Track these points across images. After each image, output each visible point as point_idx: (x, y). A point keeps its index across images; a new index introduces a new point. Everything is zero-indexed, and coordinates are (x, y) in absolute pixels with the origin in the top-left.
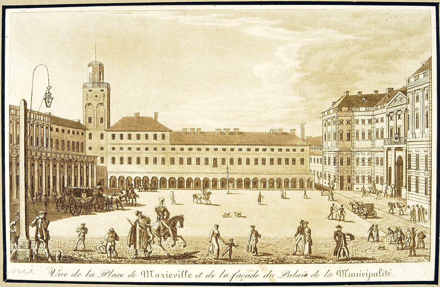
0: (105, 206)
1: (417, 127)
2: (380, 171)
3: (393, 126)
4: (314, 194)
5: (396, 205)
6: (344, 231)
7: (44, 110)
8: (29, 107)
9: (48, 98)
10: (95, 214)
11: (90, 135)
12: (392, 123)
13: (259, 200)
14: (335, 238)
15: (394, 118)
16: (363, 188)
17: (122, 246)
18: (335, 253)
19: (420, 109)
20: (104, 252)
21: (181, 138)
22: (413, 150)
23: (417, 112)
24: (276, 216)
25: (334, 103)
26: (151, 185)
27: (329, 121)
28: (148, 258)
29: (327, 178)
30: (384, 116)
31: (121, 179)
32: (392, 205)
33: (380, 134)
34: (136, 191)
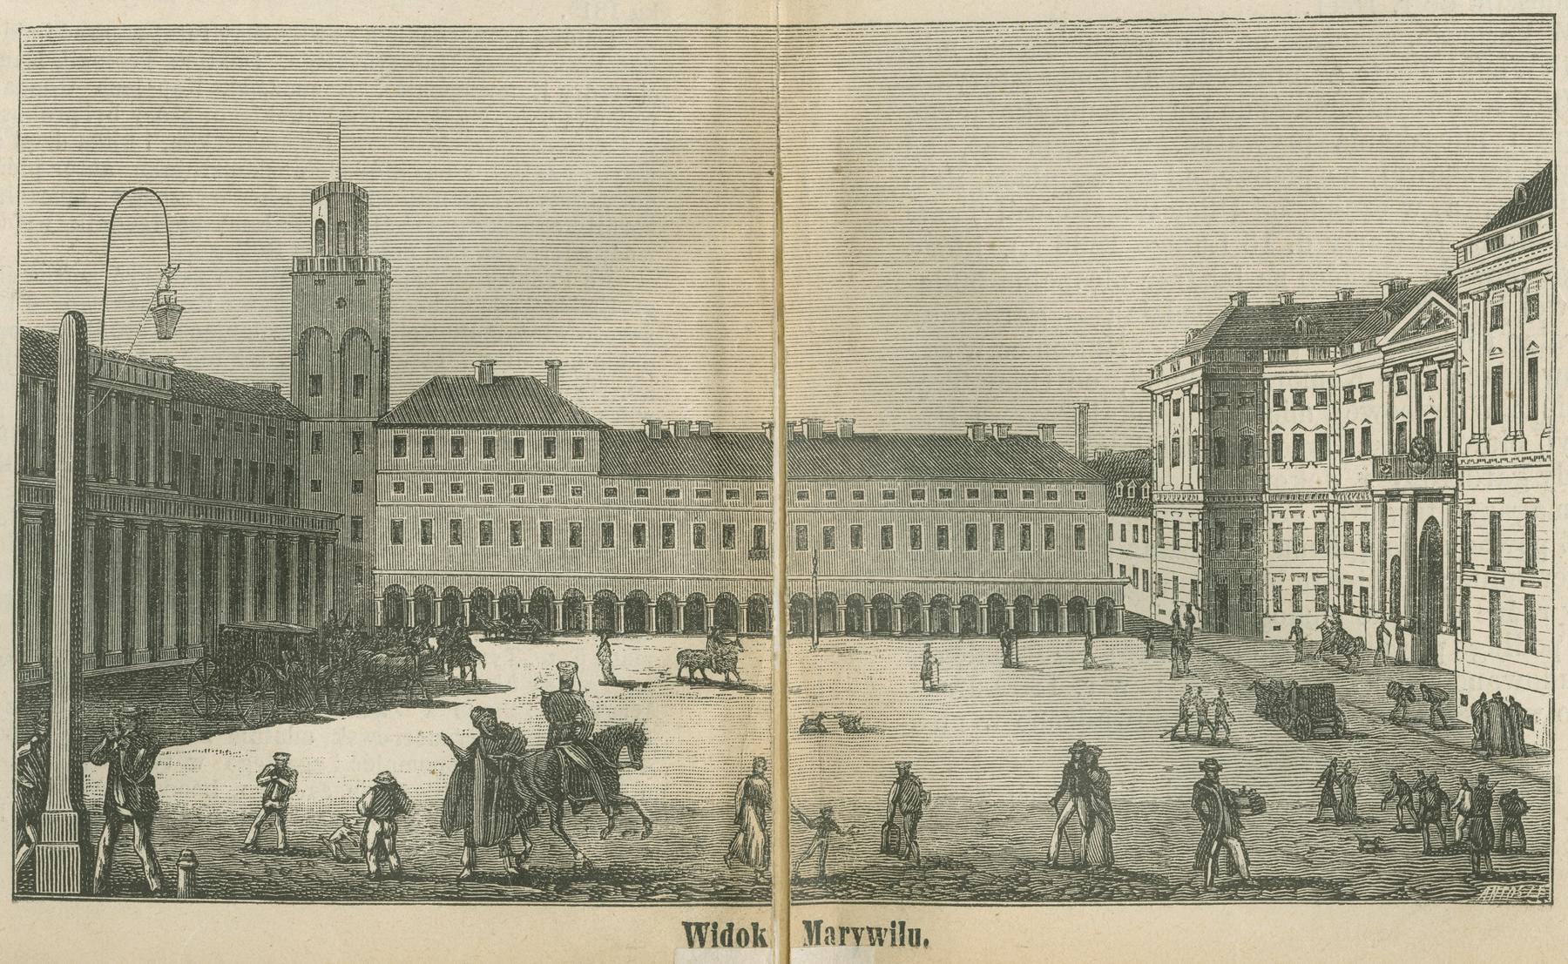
0: (372, 691)
1: (1533, 417)
2: (1359, 568)
3: (1437, 409)
4: (1124, 653)
5: (1417, 691)
6: (1229, 780)
7: (149, 348)
8: (93, 340)
9: (166, 313)
10: (327, 720)
11: (317, 438)
12: (1402, 404)
13: (925, 676)
14: (1197, 806)
15: (1410, 383)
16: (1297, 630)
17: (420, 837)
18: (1200, 865)
19: (1506, 350)
20: (358, 855)
21: (642, 453)
22: (1482, 498)
23: (1496, 363)
24: (983, 726)
25: (1197, 332)
26: (530, 618)
27: (1177, 395)
28: (522, 878)
29: (1169, 593)
30: (1374, 376)
31: (424, 599)
32: (1401, 694)
33: (1356, 442)
34: (475, 638)
